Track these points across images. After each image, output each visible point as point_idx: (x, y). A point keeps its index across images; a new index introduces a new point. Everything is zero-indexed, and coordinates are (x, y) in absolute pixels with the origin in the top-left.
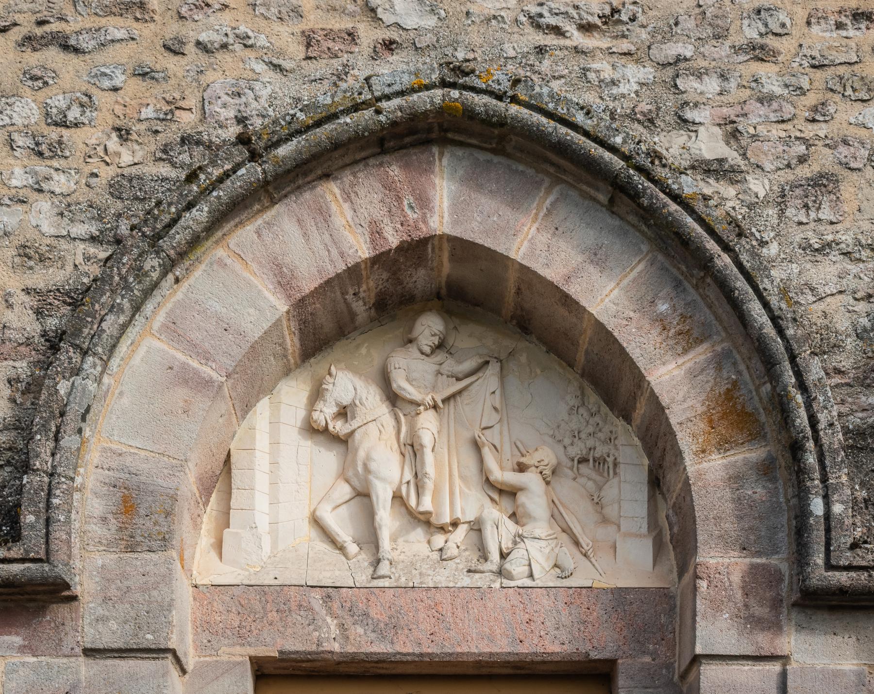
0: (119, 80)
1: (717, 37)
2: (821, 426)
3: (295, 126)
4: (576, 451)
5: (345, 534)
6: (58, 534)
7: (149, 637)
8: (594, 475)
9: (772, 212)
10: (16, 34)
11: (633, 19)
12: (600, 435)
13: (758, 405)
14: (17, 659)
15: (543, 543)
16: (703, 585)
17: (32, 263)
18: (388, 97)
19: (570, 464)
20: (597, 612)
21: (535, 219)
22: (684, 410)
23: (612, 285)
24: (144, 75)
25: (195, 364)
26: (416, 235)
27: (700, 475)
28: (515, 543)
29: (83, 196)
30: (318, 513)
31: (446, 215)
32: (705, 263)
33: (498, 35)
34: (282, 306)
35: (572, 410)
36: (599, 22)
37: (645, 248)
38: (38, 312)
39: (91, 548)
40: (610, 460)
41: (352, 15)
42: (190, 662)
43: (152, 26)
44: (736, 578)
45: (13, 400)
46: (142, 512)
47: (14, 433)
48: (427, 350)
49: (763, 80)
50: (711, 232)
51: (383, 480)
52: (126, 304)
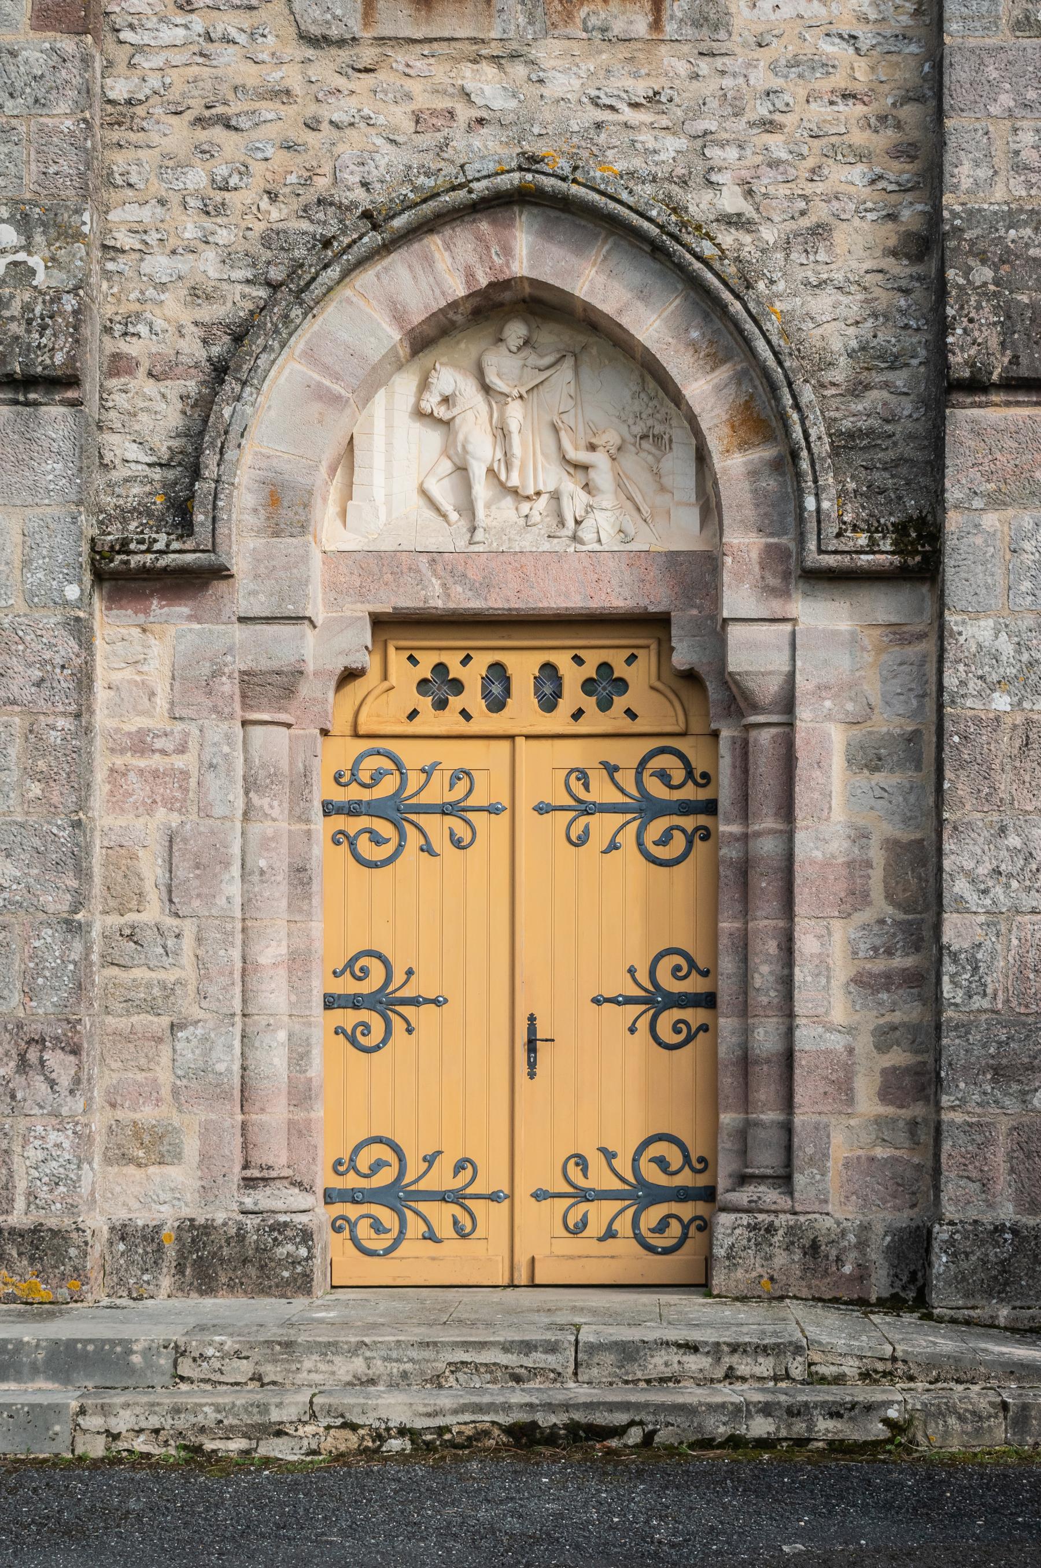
0: (269, 152)
1: (736, 115)
2: (812, 439)
3: (406, 204)
4: (639, 429)
5: (447, 507)
6: (222, 530)
7: (290, 607)
8: (653, 450)
9: (780, 256)
10: (189, 116)
11: (671, 100)
12: (658, 416)
13: (770, 413)
14: (186, 626)
15: (609, 514)
16: (728, 560)
17: (200, 301)
18: (478, 180)
19: (632, 440)
20: (654, 573)
21: (594, 265)
22: (712, 418)
23: (655, 316)
24: (289, 148)
25: (327, 382)
26: (501, 278)
27: (725, 470)
28: (587, 512)
29: (241, 246)
30: (425, 486)
31: (525, 261)
32: (722, 308)
33: (566, 113)
34: (396, 336)
35: (635, 396)
36: (644, 102)
37: (680, 287)
38: (205, 341)
39: (244, 534)
40: (666, 437)
41: (452, 96)
42: (319, 621)
43: (295, 107)
44: (755, 555)
45: (184, 413)
46: (286, 504)
47: (184, 440)
48: (514, 349)
49: (773, 148)
50: (725, 284)
51: (478, 459)
52: (276, 345)
